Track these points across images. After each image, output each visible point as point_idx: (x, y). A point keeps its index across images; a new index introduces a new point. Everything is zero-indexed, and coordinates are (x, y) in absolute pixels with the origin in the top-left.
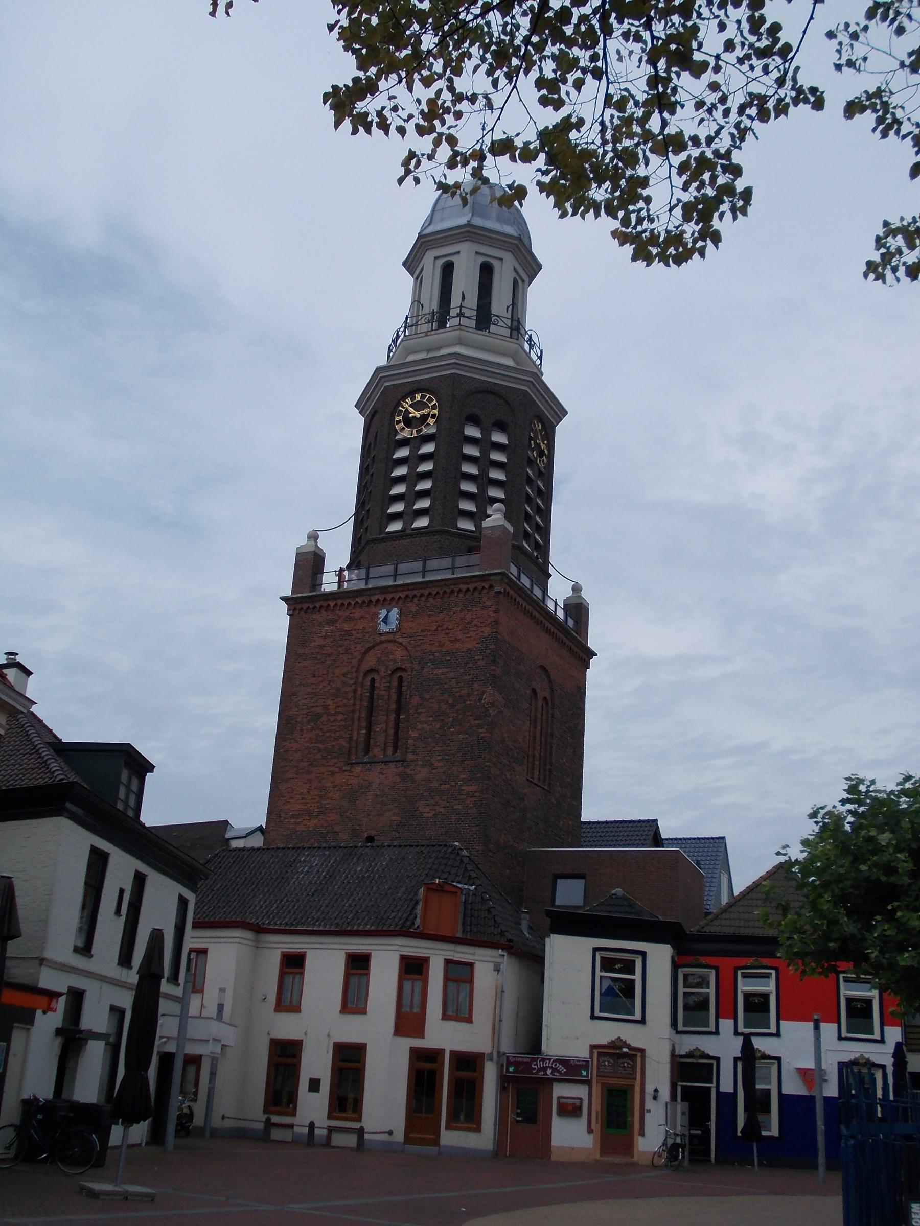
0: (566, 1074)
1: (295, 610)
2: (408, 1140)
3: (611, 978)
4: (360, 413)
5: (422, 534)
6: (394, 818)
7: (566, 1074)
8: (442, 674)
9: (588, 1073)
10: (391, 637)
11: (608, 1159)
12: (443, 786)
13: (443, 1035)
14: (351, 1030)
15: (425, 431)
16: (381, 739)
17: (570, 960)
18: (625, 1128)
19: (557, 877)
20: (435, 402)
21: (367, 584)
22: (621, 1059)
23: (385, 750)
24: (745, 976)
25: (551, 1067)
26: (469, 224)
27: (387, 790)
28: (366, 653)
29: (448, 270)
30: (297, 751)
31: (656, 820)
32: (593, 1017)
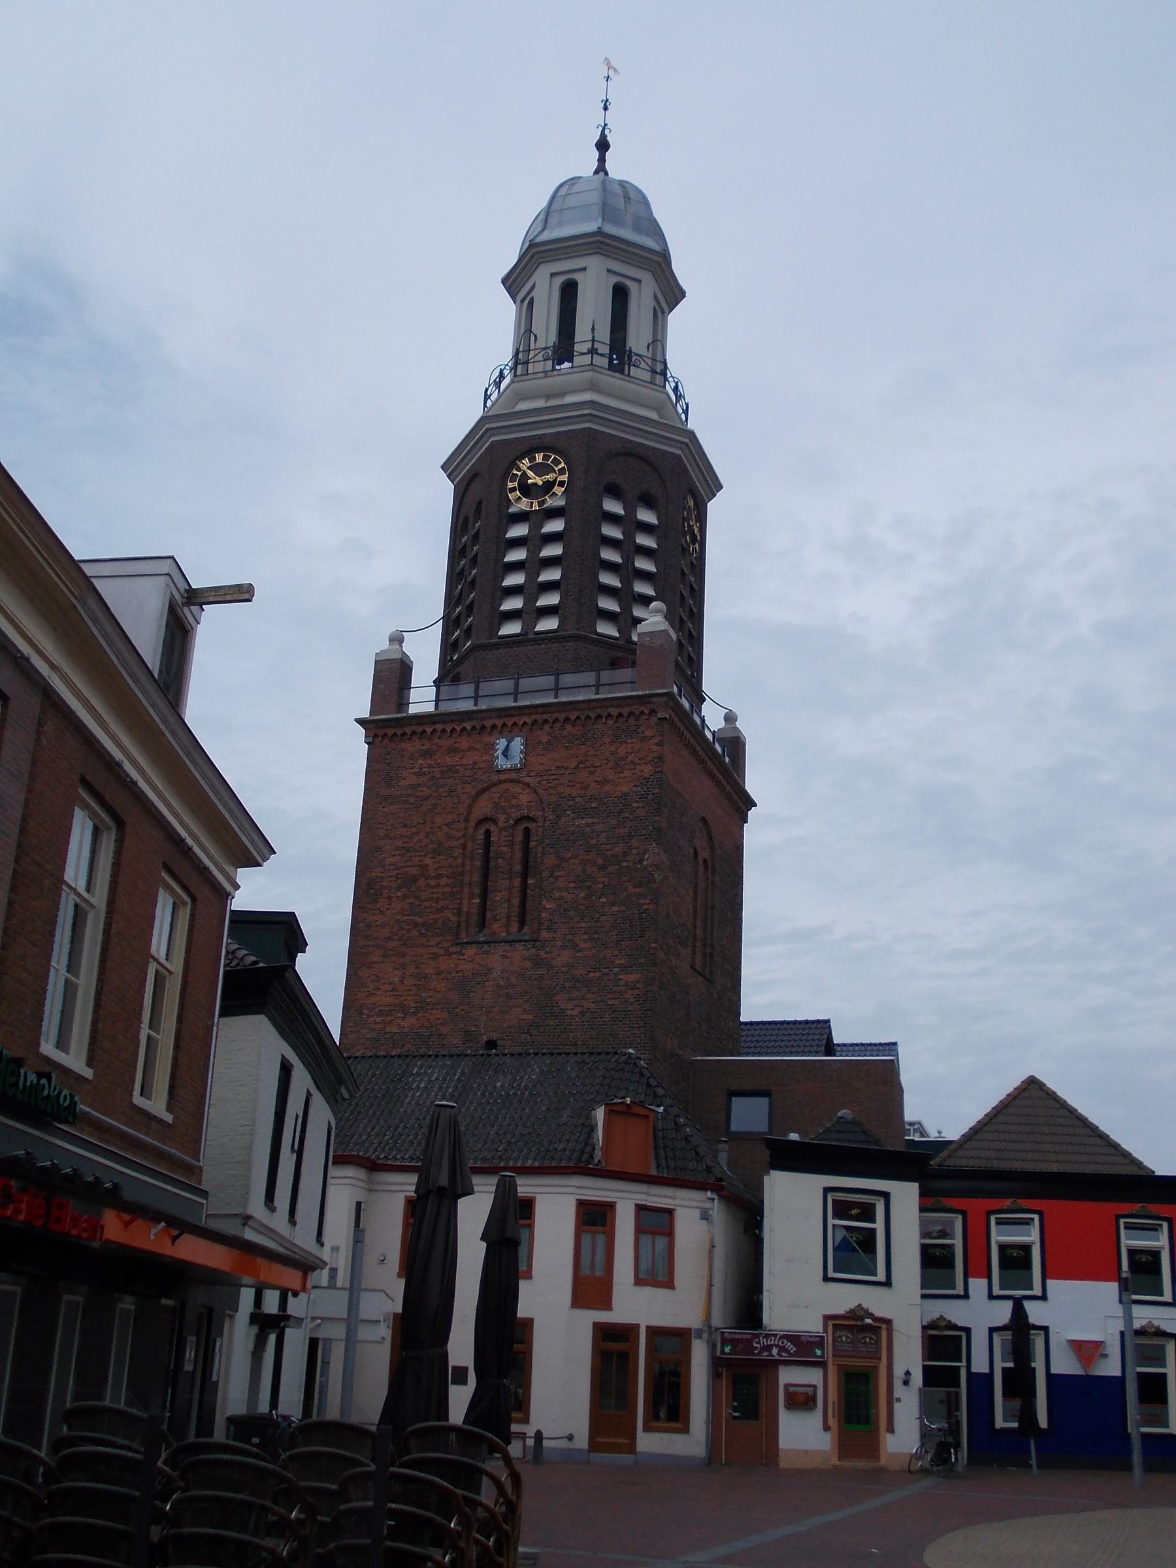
0: (796, 1354)
1: (376, 736)
2: (594, 1446)
3: (847, 1228)
4: (448, 477)
5: (550, 639)
6: (525, 1016)
7: (796, 1354)
8: (587, 825)
9: (823, 1353)
10: (514, 775)
11: (849, 1464)
12: (591, 975)
13: (635, 1305)
15: (550, 502)
16: (502, 911)
17: (795, 1205)
18: (867, 1422)
19: (733, 1094)
20: (562, 465)
21: (476, 705)
22: (861, 1332)
23: (507, 925)
24: (999, 1222)
25: (777, 1346)
26: (599, 232)
27: (513, 980)
28: (478, 795)
29: (569, 292)
30: (383, 925)
31: (828, 1021)
32: (826, 1279)
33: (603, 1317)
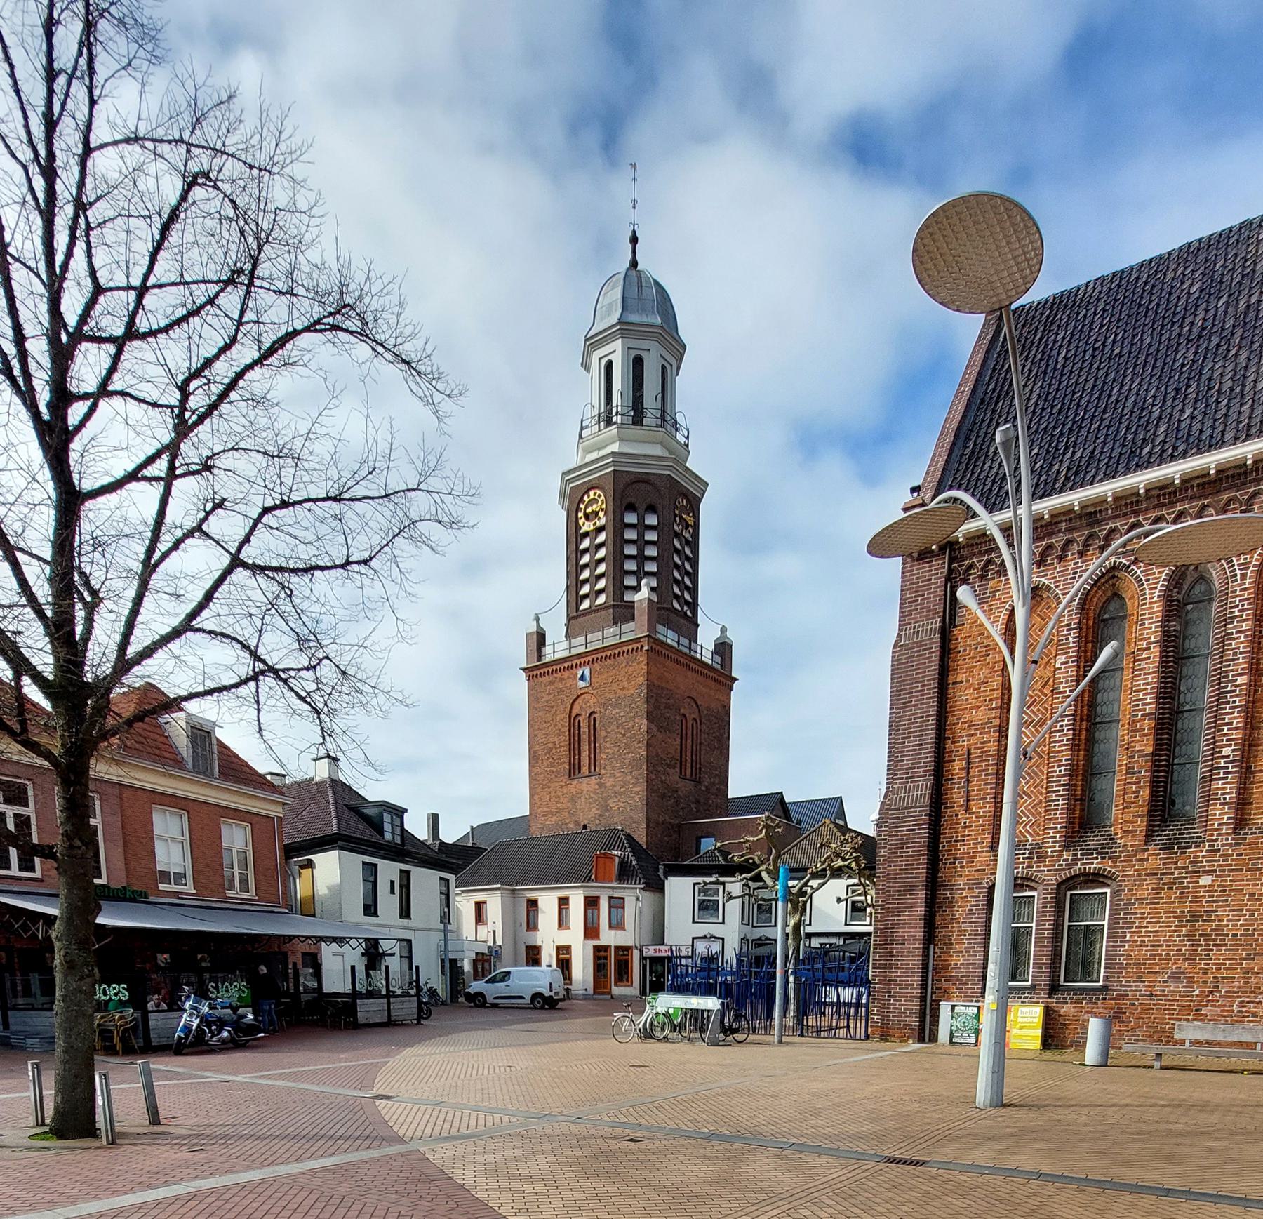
2: (595, 993)
13: (609, 937)
14: (563, 938)
32: (723, 922)
33: (597, 943)
